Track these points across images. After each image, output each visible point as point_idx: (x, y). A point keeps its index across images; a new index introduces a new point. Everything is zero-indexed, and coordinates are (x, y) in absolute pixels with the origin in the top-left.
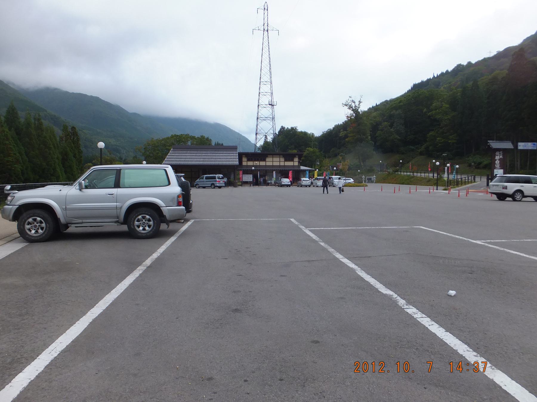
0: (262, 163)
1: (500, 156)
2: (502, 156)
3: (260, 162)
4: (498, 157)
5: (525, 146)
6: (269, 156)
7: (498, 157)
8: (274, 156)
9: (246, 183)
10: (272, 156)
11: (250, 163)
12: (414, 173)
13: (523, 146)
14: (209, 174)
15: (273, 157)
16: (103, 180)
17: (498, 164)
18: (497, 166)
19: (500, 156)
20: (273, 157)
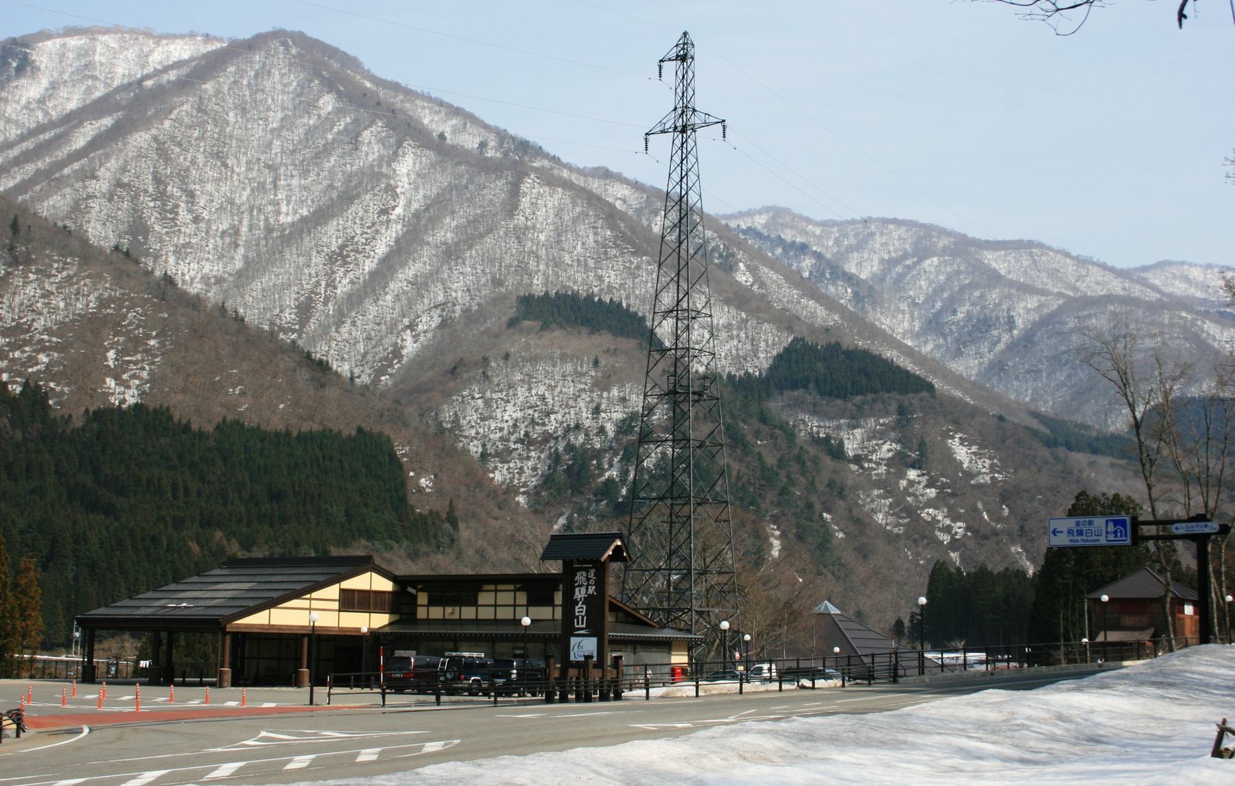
0: (468, 613)
1: (587, 589)
2: (594, 587)
3: (463, 608)
4: (583, 590)
5: (1080, 533)
6: (486, 587)
7: (583, 590)
8: (500, 587)
9: (760, 212)
10: (492, 587)
11: (436, 613)
12: (651, 690)
13: (1070, 532)
14: (101, 781)
15: (496, 591)
16: (901, 737)
17: (583, 617)
18: (580, 626)
19: (587, 589)
20: (496, 591)
